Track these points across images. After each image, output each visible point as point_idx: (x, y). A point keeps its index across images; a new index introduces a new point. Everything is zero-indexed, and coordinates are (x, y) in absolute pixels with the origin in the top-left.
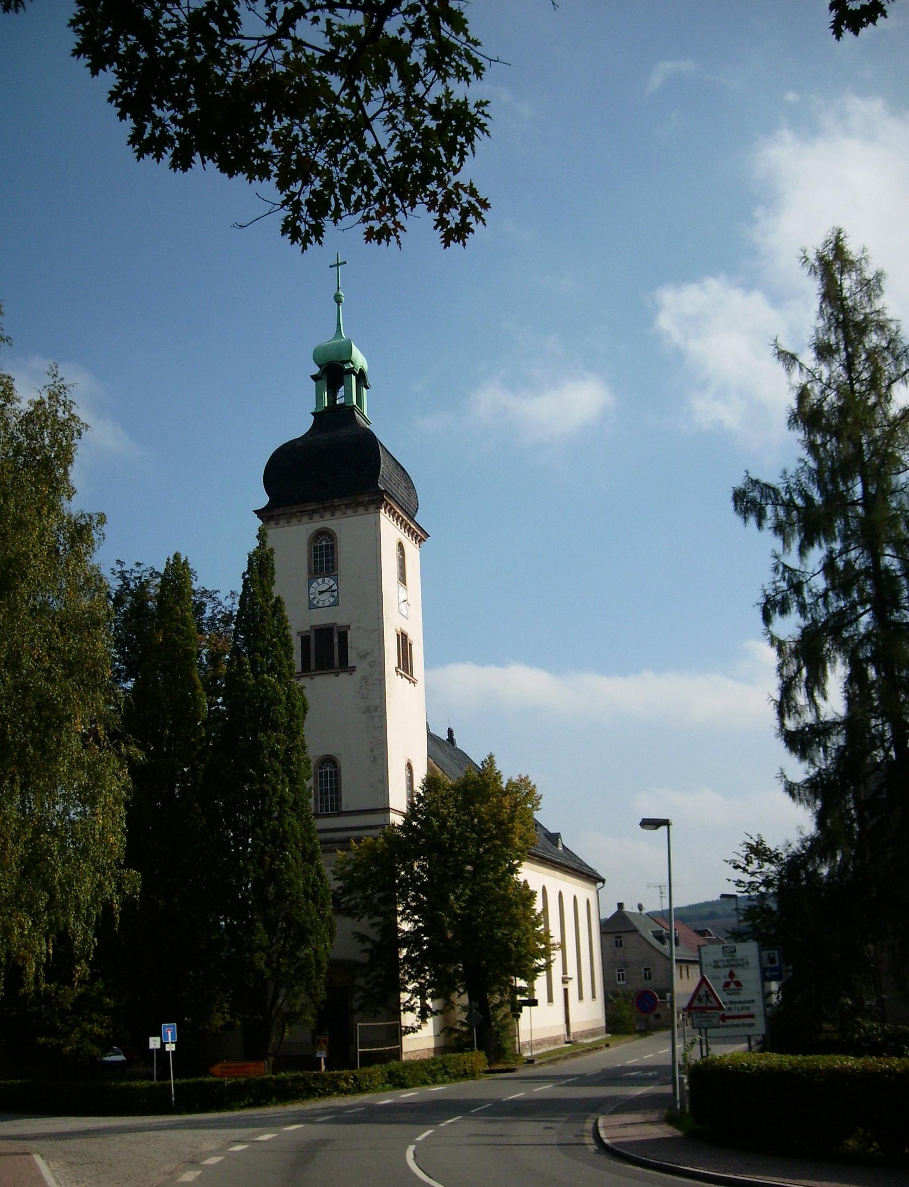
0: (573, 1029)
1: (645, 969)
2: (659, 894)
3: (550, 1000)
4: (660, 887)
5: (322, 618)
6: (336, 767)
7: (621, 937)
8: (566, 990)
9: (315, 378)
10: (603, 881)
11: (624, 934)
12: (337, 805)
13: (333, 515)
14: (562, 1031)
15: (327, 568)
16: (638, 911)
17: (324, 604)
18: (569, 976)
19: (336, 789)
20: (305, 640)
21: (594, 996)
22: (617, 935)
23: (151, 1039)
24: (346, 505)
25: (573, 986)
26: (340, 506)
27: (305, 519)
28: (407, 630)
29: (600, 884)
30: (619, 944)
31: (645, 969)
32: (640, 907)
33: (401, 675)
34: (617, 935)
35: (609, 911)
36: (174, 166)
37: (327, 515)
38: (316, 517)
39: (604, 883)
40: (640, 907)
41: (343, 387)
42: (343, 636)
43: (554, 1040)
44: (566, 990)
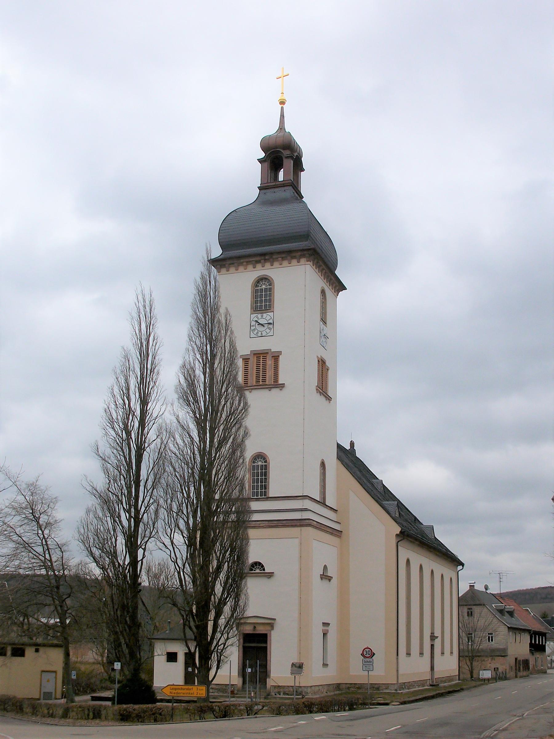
0: (436, 676)
1: (489, 634)
2: (498, 579)
3: (421, 654)
4: (499, 574)
5: (261, 345)
6: (266, 462)
7: (472, 609)
8: (432, 646)
9: (261, 161)
10: (463, 565)
11: (474, 607)
12: (265, 492)
13: (272, 265)
14: (428, 677)
15: (266, 306)
16: (484, 590)
17: (262, 333)
18: (436, 635)
19: (266, 472)
20: (246, 360)
21: (421, 654)
22: (470, 607)
23: (189, 668)
24: (282, 258)
25: (437, 643)
26: (277, 258)
27: (250, 267)
28: (325, 358)
29: (460, 567)
30: (470, 614)
31: (489, 634)
32: (486, 588)
33: (320, 393)
34: (470, 607)
35: (464, 588)
36: (250, 568)
37: (268, 265)
38: (259, 266)
39: (463, 566)
40: (486, 588)
41: (282, 170)
42: (276, 357)
43: (422, 683)
44: (432, 646)
